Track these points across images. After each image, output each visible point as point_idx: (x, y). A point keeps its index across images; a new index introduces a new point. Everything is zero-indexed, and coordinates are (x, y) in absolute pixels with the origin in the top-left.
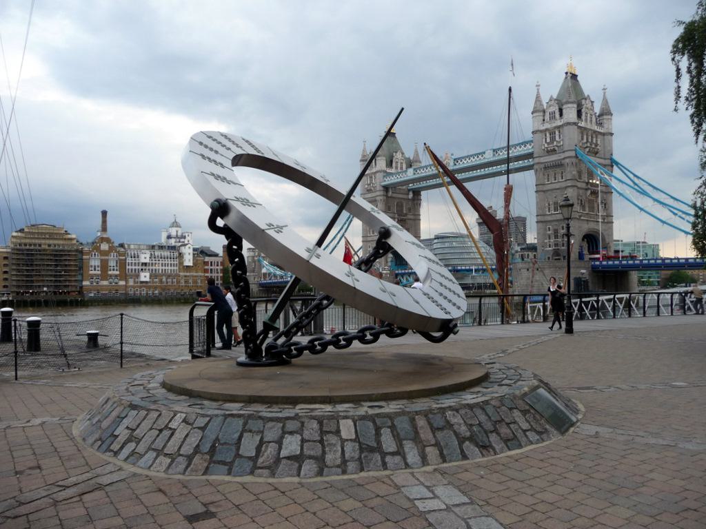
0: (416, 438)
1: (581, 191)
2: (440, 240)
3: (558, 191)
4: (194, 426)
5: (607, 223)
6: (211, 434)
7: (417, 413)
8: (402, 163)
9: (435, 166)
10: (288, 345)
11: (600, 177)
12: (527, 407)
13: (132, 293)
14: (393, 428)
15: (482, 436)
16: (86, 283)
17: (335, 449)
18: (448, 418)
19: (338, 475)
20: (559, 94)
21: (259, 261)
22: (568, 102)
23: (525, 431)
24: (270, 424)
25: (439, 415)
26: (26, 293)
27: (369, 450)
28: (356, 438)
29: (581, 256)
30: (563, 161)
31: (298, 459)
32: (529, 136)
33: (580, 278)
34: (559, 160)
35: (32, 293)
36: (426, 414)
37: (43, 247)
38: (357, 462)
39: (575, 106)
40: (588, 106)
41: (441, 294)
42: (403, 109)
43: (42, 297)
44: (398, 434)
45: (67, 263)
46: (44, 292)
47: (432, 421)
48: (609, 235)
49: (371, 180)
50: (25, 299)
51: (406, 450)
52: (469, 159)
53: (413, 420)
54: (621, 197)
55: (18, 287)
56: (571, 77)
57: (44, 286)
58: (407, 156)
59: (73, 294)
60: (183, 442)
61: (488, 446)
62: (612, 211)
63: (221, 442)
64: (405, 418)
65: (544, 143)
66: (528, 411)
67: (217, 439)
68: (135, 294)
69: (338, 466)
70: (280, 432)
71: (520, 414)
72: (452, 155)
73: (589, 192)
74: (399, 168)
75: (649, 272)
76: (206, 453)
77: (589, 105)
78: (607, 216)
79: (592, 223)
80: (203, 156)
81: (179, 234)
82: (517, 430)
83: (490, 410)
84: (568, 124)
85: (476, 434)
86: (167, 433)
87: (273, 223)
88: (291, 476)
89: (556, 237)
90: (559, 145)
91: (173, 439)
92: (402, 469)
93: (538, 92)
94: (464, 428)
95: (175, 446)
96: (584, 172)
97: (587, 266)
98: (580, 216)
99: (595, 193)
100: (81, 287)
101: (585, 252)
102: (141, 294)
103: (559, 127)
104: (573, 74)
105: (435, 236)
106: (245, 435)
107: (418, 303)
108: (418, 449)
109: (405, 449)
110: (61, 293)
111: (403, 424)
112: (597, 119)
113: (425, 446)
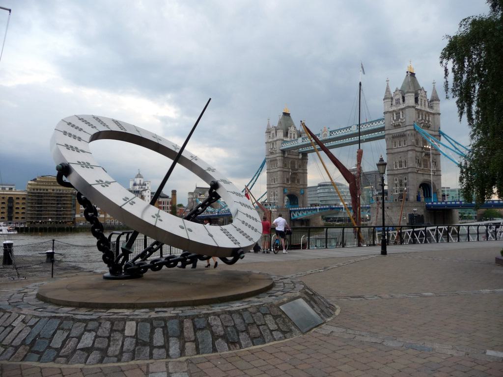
0: (181, 336)
1: (418, 154)
2: (322, 187)
3: (402, 153)
4: (27, 325)
5: (437, 175)
6: (35, 331)
7: (186, 317)
8: (294, 134)
9: (310, 139)
10: (139, 264)
11: (432, 144)
12: (280, 313)
13: (109, 222)
14: (165, 328)
15: (234, 335)
16: (77, 216)
17: (118, 343)
18: (209, 321)
19: (114, 362)
20: (402, 87)
21: (196, 201)
22: (408, 92)
23: (271, 331)
24: (77, 324)
25: (204, 319)
26: (38, 222)
27: (143, 344)
28: (135, 335)
29: (418, 199)
30: (405, 133)
31: (88, 350)
32: (382, 116)
33: (413, 214)
34: (403, 132)
35: (41, 223)
36: (193, 318)
37: (49, 191)
38: (131, 353)
39: (414, 95)
40: (422, 95)
41: (81, 130)
42: (210, 99)
43: (47, 226)
44: (168, 332)
45: (65, 202)
46: (49, 222)
47: (196, 323)
48: (438, 184)
49: (273, 146)
50: (36, 226)
51: (171, 344)
52: (341, 131)
53: (181, 323)
54: (446, 157)
55: (32, 218)
56: (411, 75)
57: (49, 218)
58: (298, 130)
59: (69, 223)
60: (16, 336)
61: (236, 343)
62: (440, 167)
63: (41, 337)
64: (176, 321)
65: (392, 120)
66: (280, 316)
67: (39, 334)
68: (111, 223)
69: (116, 356)
70: (83, 329)
71: (271, 318)
72: (329, 128)
73: (424, 154)
74: (292, 138)
75: (469, 210)
76: (28, 345)
77: (423, 94)
78: (437, 171)
79: (426, 176)
80: (65, 133)
81: (142, 183)
82: (264, 330)
83: (246, 315)
84: (409, 107)
85: (229, 334)
86: (8, 329)
87: (102, 180)
88: (80, 363)
89: (401, 185)
90: (402, 121)
91: (10, 334)
92: (163, 359)
93: (388, 85)
94: (221, 328)
95: (10, 339)
96: (420, 140)
97: (423, 206)
98: (418, 171)
99: (428, 155)
100: (74, 219)
101: (422, 196)
102: (111, 223)
103: (402, 109)
104: (412, 73)
105: (319, 184)
106: (58, 331)
107: (211, 236)
108: (180, 343)
109: (170, 344)
110: (60, 223)
111: (173, 326)
112: (429, 104)
113: (186, 342)
